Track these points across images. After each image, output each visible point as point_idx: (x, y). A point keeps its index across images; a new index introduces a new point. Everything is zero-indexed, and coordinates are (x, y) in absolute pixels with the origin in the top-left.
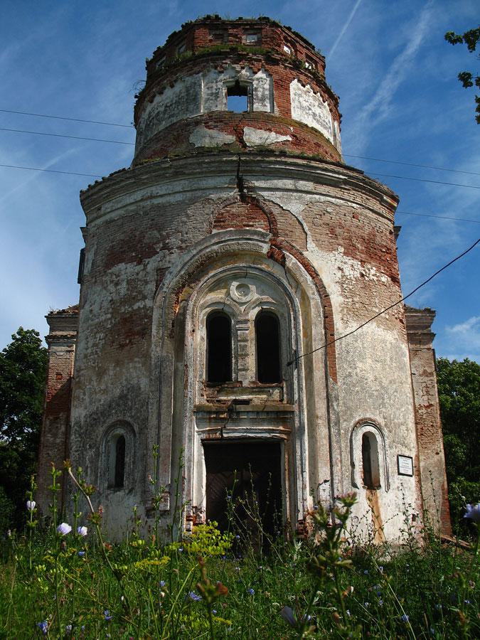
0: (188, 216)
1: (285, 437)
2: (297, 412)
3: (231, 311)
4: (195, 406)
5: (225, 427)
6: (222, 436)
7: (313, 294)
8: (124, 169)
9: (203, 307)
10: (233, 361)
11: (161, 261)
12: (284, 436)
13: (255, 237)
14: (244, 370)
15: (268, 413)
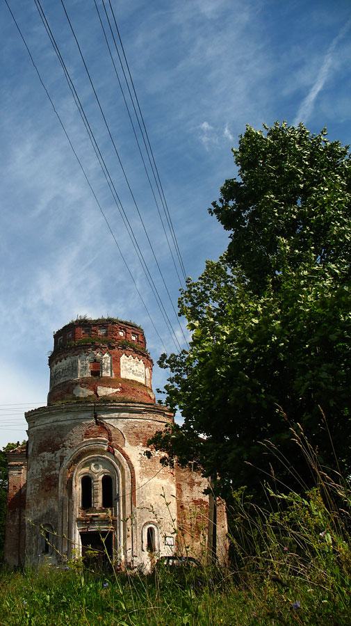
9: (80, 475)
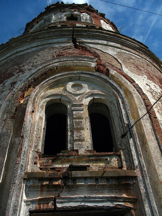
0: (38, 55)
1: (131, 206)
2: (140, 178)
3: (67, 99)
4: (26, 173)
5: (59, 196)
6: (55, 205)
7: (134, 90)
8: (3, 44)
9: (43, 98)
10: (69, 134)
11: (16, 78)
12: (129, 205)
13: (86, 59)
14: (80, 140)
15: (108, 179)
